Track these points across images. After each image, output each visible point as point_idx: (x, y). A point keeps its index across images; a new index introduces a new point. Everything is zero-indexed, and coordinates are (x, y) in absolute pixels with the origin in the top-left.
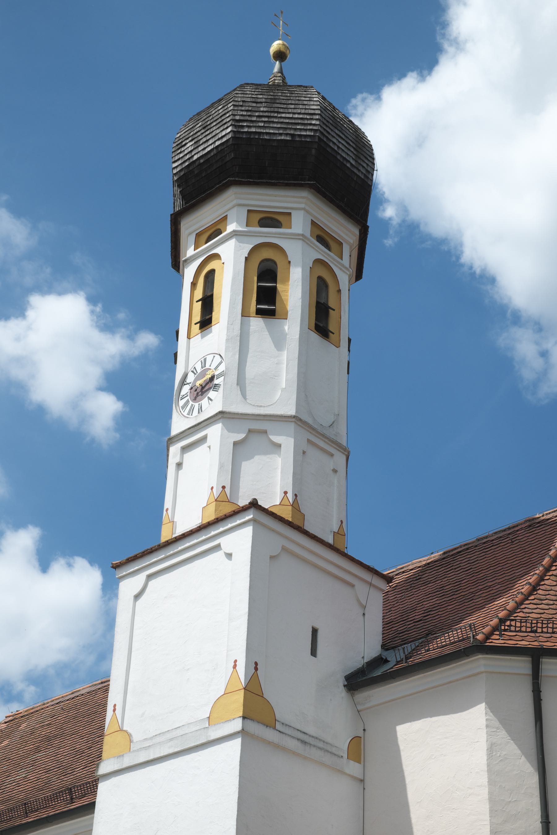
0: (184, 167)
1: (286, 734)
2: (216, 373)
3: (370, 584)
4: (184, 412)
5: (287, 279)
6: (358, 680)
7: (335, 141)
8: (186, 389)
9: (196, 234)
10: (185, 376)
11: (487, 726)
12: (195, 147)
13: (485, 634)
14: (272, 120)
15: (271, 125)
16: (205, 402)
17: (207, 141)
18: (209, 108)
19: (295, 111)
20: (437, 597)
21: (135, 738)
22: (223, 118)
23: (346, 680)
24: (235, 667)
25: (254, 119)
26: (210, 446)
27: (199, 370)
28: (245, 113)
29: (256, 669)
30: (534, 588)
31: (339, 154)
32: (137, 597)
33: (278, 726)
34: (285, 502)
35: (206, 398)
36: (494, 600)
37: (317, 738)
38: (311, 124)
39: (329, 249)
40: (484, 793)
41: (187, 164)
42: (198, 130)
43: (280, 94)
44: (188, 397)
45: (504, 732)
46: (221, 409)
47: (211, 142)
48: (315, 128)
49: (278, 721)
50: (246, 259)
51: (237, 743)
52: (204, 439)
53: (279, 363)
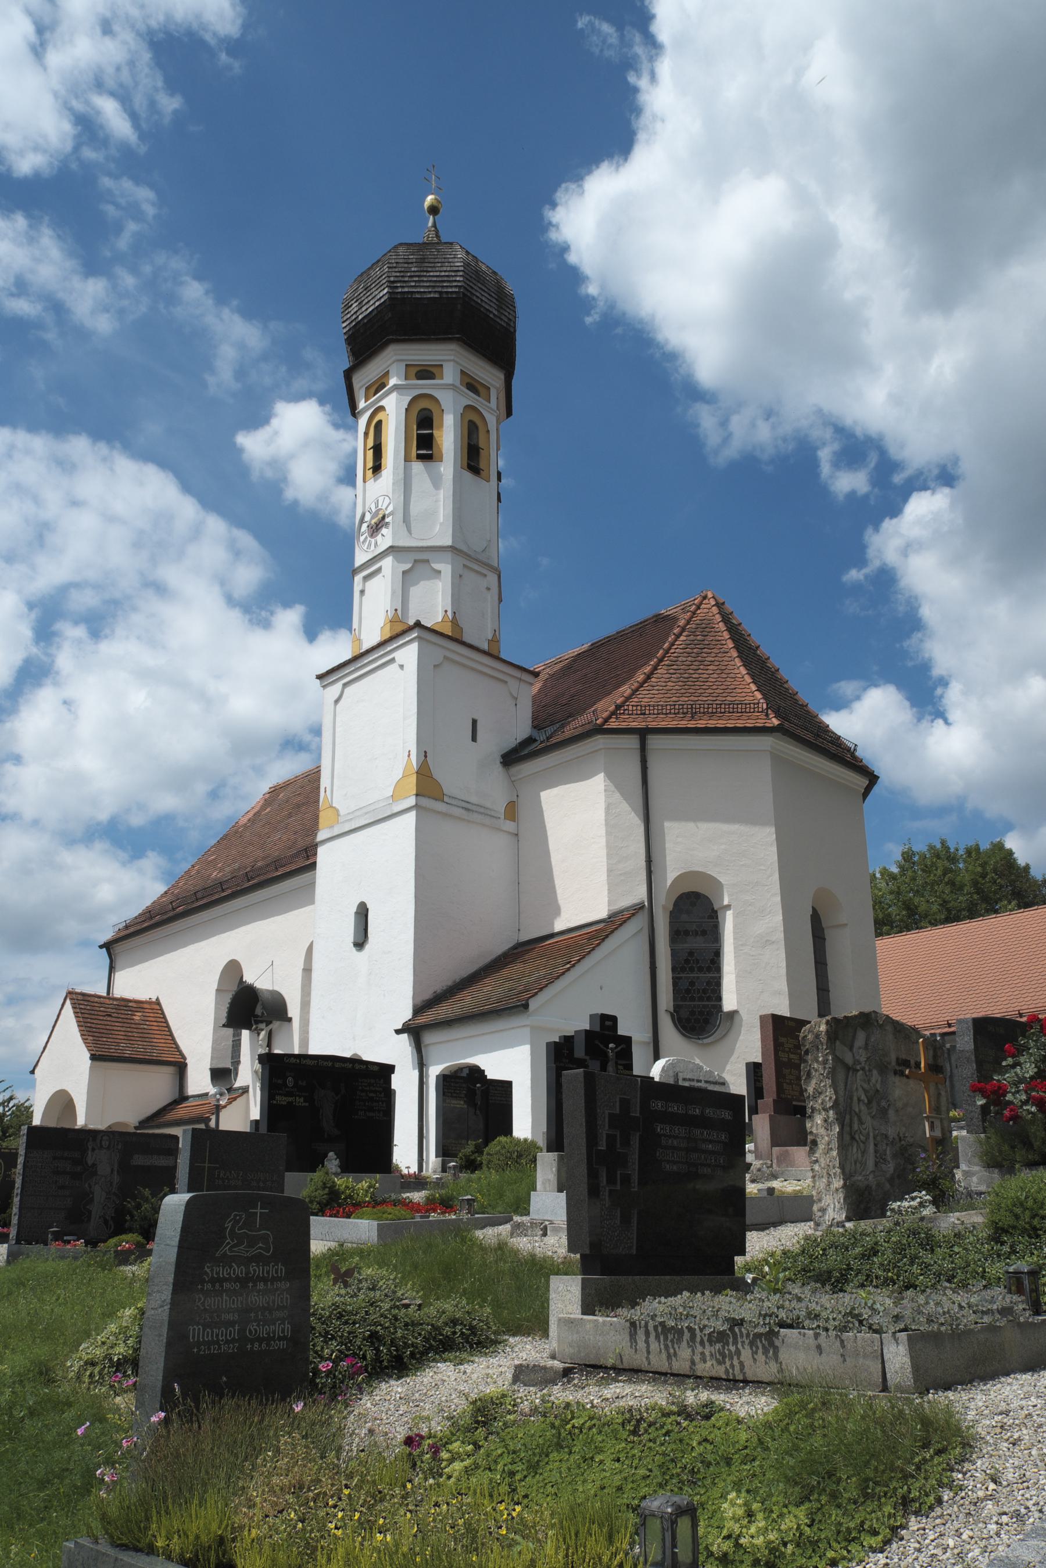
2: (387, 513)
3: (520, 680)
5: (441, 426)
7: (478, 295)
8: (364, 527)
10: (363, 516)
11: (605, 791)
14: (422, 279)
15: (422, 284)
16: (379, 538)
17: (369, 301)
18: (369, 269)
19: (442, 269)
21: (342, 812)
25: (406, 279)
27: (374, 510)
28: (398, 274)
29: (426, 756)
30: (648, 677)
32: (337, 701)
33: (446, 799)
34: (446, 619)
36: (619, 687)
38: (456, 281)
39: (479, 395)
40: (603, 841)
41: (354, 323)
45: (618, 794)
46: (389, 544)
47: (372, 302)
48: (459, 284)
51: (412, 815)
52: (379, 570)
53: (437, 501)
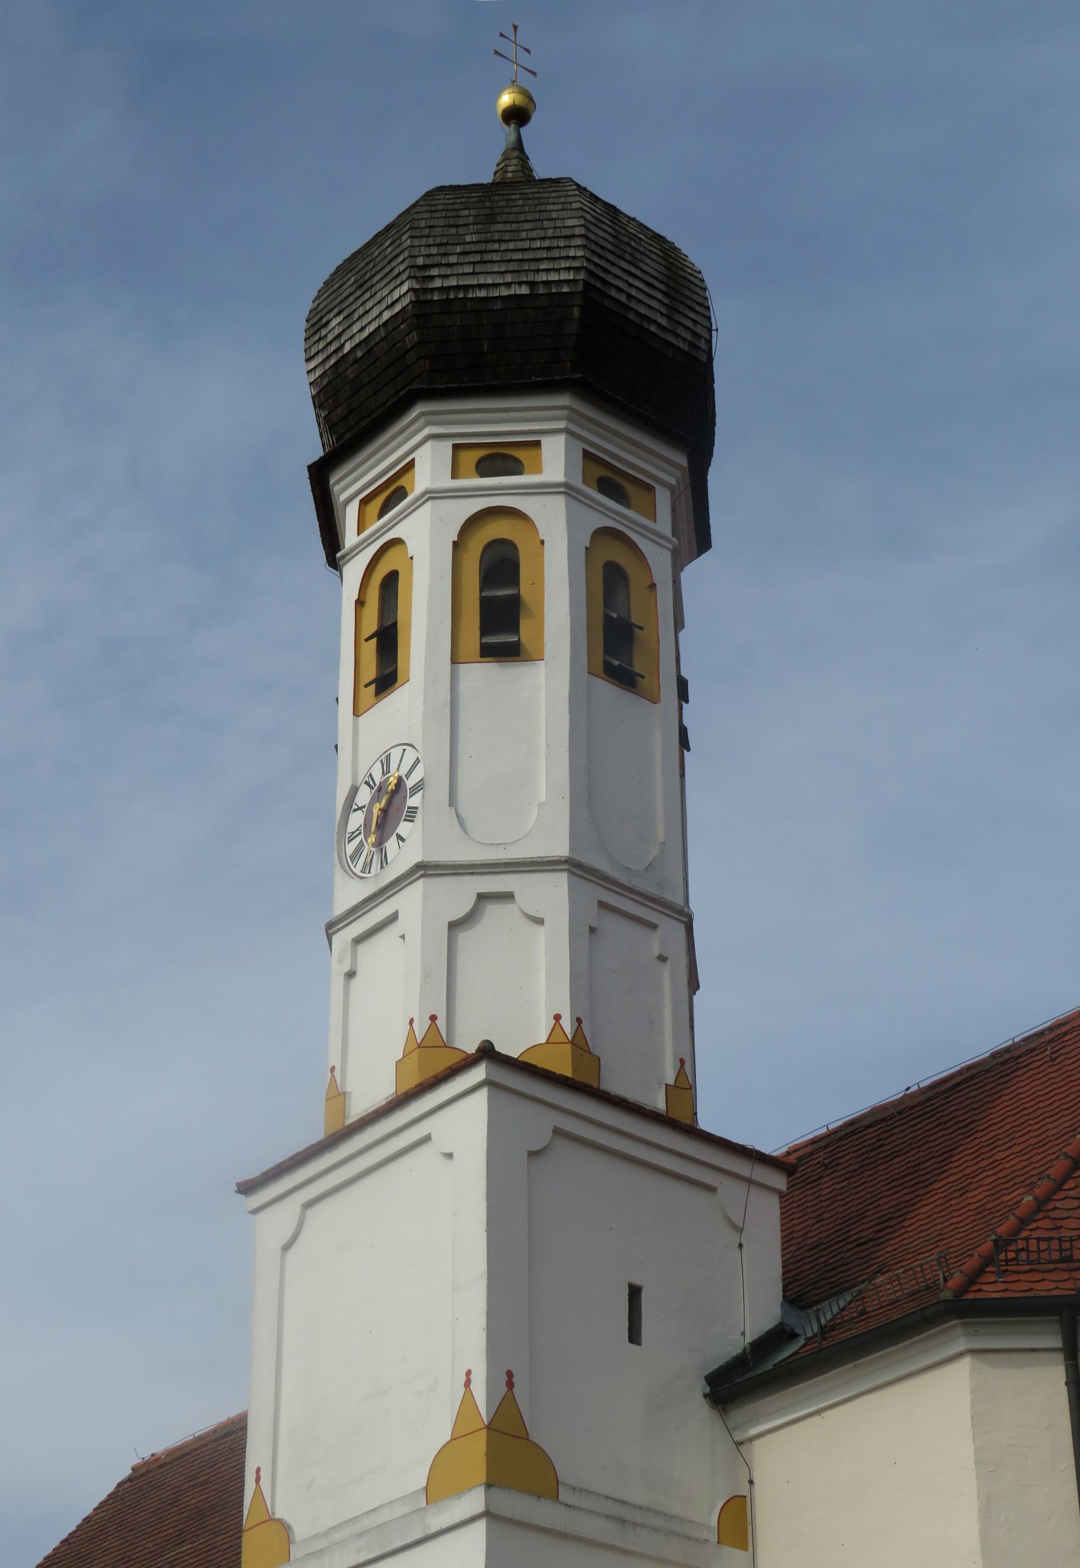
0: (327, 367)
1: (580, 1509)
3: (750, 1182)
4: (355, 867)
6: (735, 1382)
7: (621, 284)
9: (361, 501)
10: (354, 791)
12: (346, 326)
13: (966, 1275)
20: (906, 1188)
21: (300, 1532)
22: (393, 264)
23: (709, 1384)
24: (468, 1384)
25: (453, 259)
26: (404, 935)
29: (510, 1384)
31: (631, 309)
35: (394, 836)
37: (649, 1509)
38: (567, 258)
41: (333, 361)
42: (348, 291)
43: (503, 204)
44: (362, 836)
46: (417, 858)
48: (576, 264)
49: (563, 1484)
50: (455, 544)
